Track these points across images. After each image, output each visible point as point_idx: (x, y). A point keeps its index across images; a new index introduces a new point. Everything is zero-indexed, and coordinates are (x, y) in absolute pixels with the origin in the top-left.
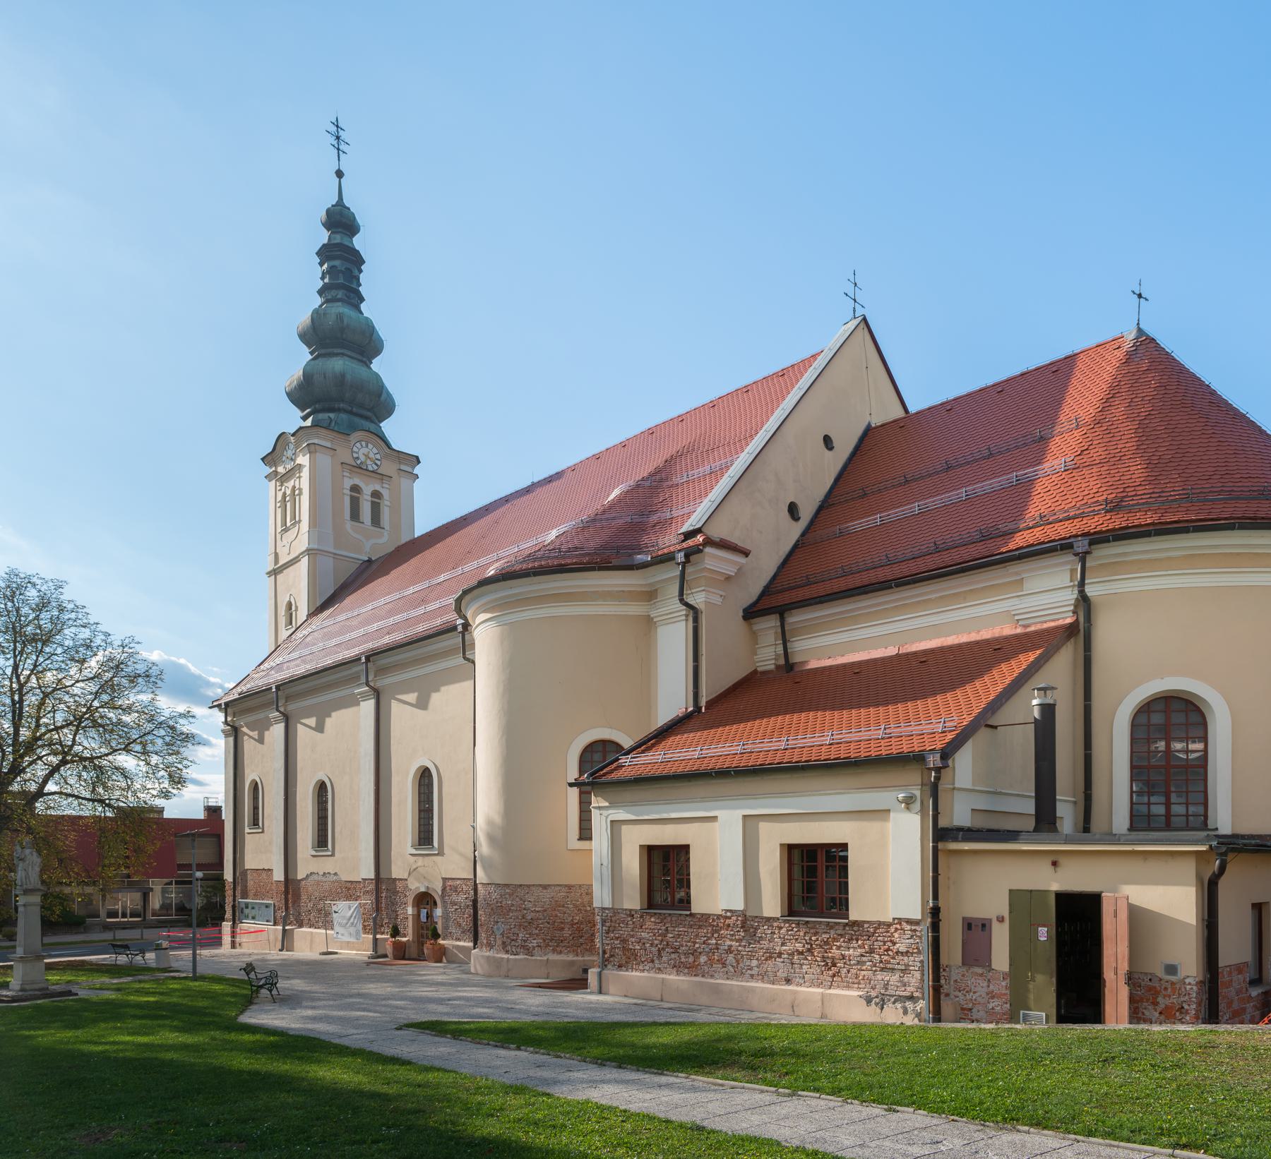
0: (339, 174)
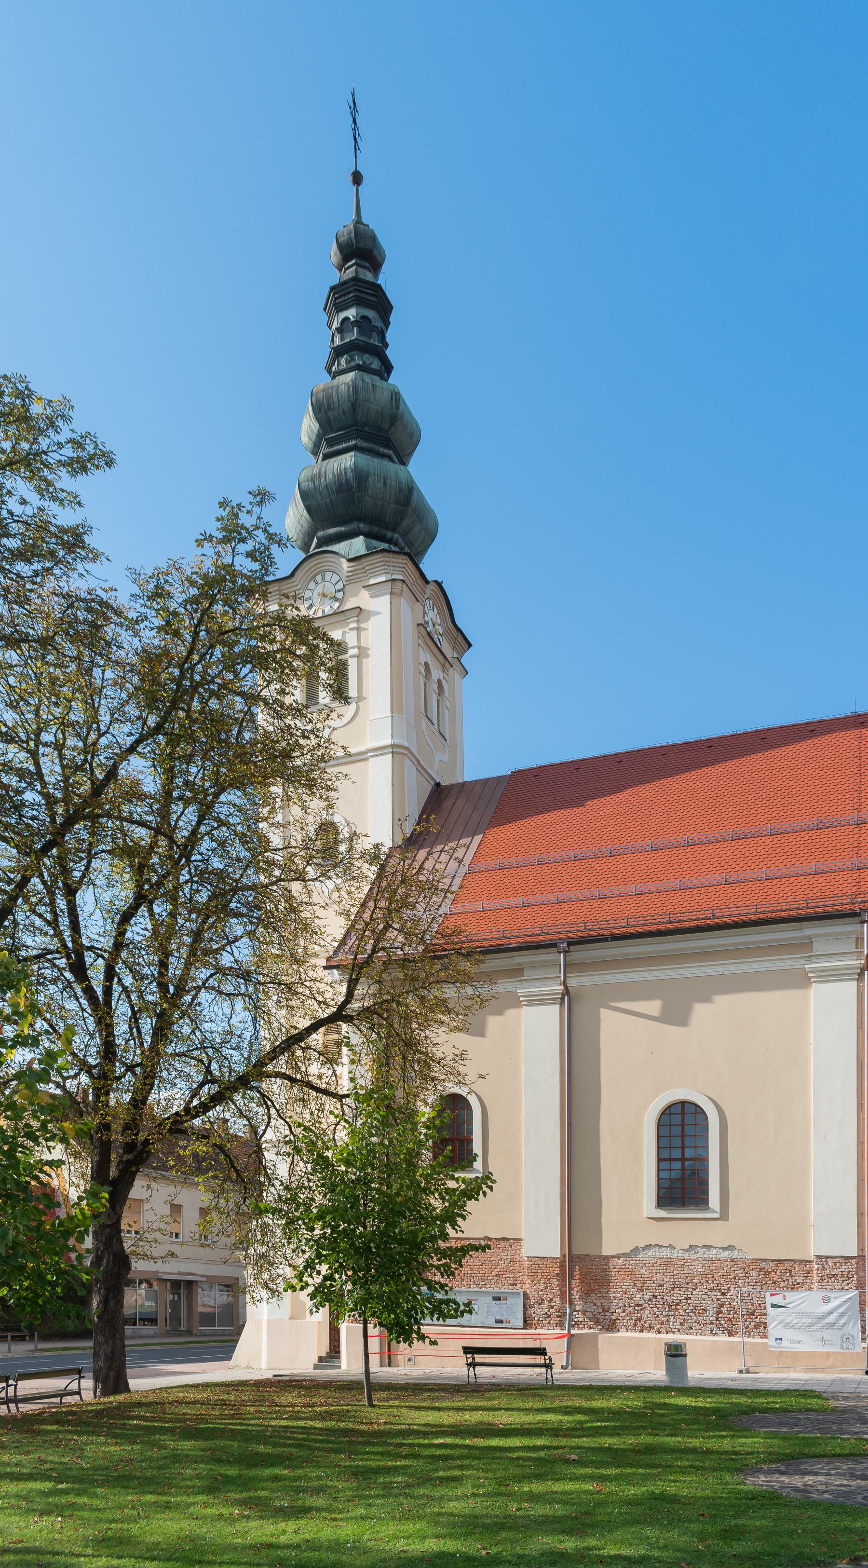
0: (357, 178)
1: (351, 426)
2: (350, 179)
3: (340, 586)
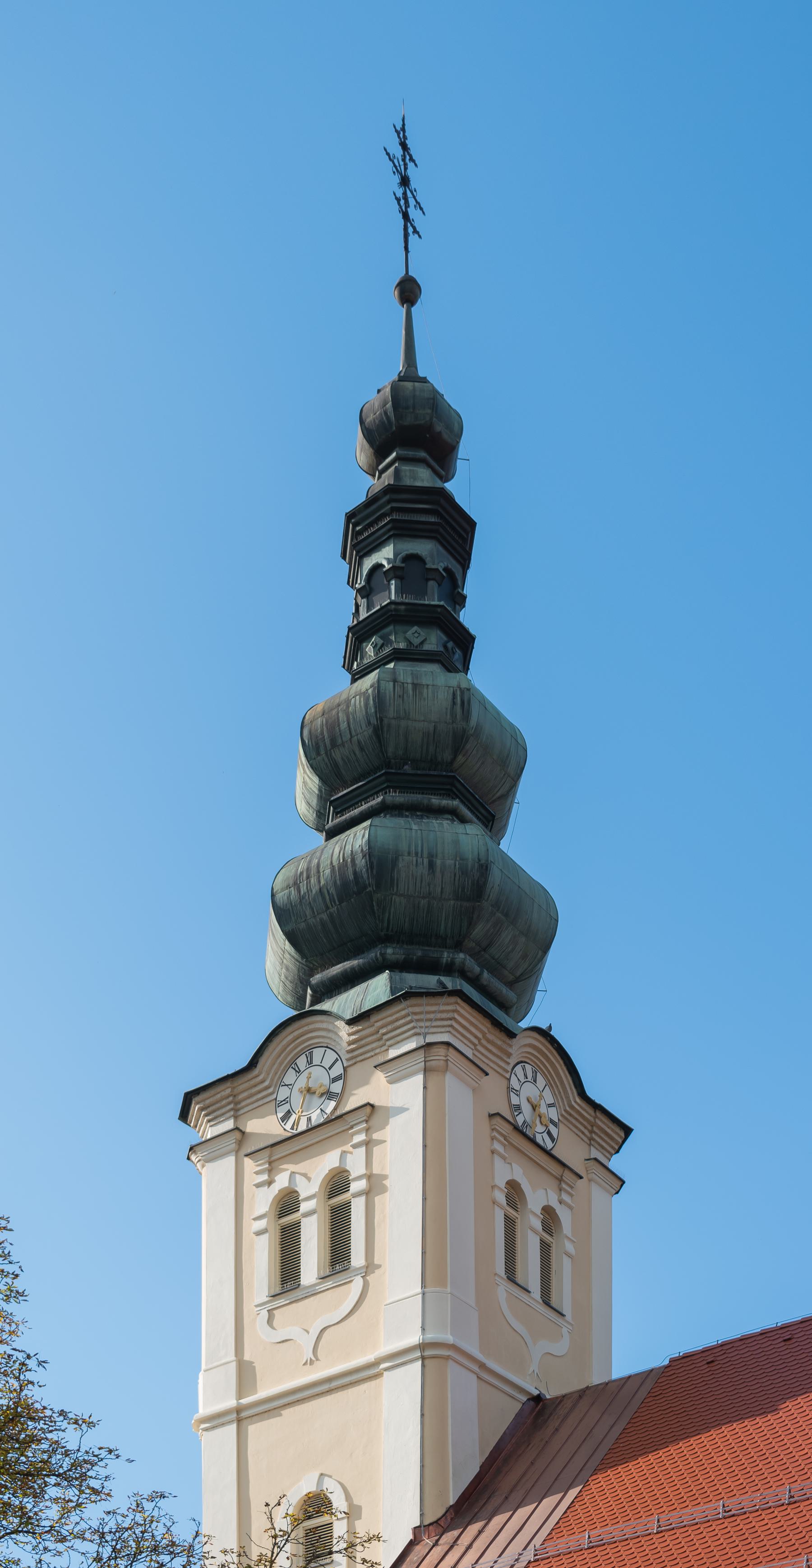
0: (408, 292)
1: (378, 769)
2: (393, 296)
3: (338, 1070)
